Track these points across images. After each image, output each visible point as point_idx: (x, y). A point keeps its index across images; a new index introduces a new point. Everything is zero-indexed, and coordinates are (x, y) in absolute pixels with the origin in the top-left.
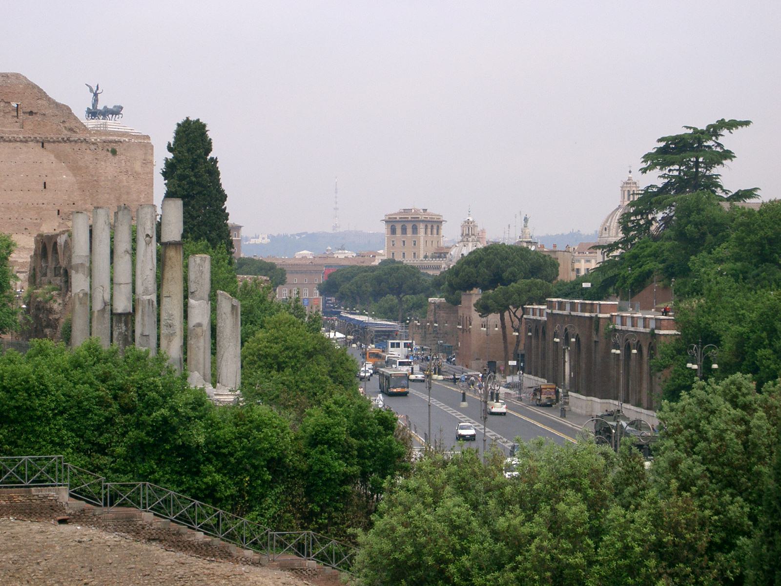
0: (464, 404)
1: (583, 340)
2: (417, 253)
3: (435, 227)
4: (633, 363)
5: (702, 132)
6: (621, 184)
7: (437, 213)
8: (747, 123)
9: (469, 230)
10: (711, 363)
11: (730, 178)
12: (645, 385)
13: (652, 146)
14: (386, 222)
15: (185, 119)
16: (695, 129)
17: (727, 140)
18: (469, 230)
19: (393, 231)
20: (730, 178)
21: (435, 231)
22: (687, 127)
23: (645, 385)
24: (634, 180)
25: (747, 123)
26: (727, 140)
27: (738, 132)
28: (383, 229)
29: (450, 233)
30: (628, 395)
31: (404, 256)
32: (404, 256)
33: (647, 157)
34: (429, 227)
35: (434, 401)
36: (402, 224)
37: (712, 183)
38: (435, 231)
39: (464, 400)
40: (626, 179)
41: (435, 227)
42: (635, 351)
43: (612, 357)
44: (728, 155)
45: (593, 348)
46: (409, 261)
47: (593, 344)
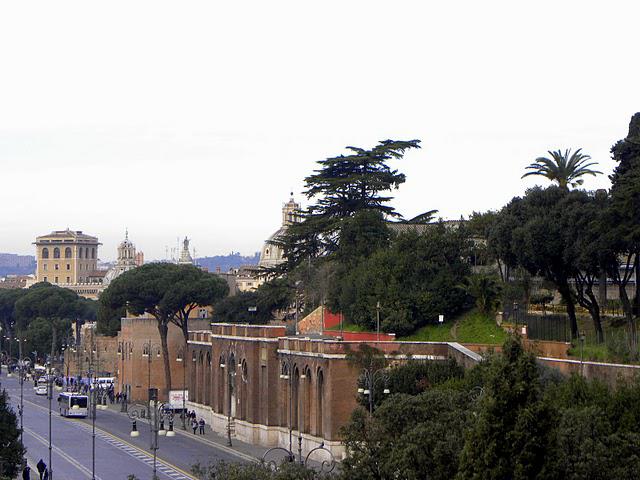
0: (134, 434)
1: (250, 365)
2: (65, 276)
3: (90, 250)
4: (301, 389)
5: (368, 153)
6: (282, 206)
7: (93, 236)
8: (413, 144)
9: (126, 248)
10: (383, 388)
11: (405, 203)
12: (314, 411)
13: (314, 168)
14: (38, 244)
15: (99, 241)
16: (361, 151)
17: (393, 164)
18: (126, 248)
19: (45, 255)
20: (405, 203)
21: (90, 255)
22: (353, 149)
23: (314, 411)
24: (296, 202)
25: (413, 144)
26: (393, 164)
27: (409, 152)
28: (34, 252)
29: (107, 254)
30: (256, 406)
31: (57, 281)
32: (57, 281)
33: (310, 180)
34: (84, 249)
35: (161, 464)
36: (55, 245)
37: (380, 209)
38: (90, 255)
39: (135, 429)
40: (288, 201)
41: (90, 250)
42: (303, 376)
43: (279, 382)
44: (401, 179)
45: (260, 373)
46: (62, 284)
47: (260, 369)
